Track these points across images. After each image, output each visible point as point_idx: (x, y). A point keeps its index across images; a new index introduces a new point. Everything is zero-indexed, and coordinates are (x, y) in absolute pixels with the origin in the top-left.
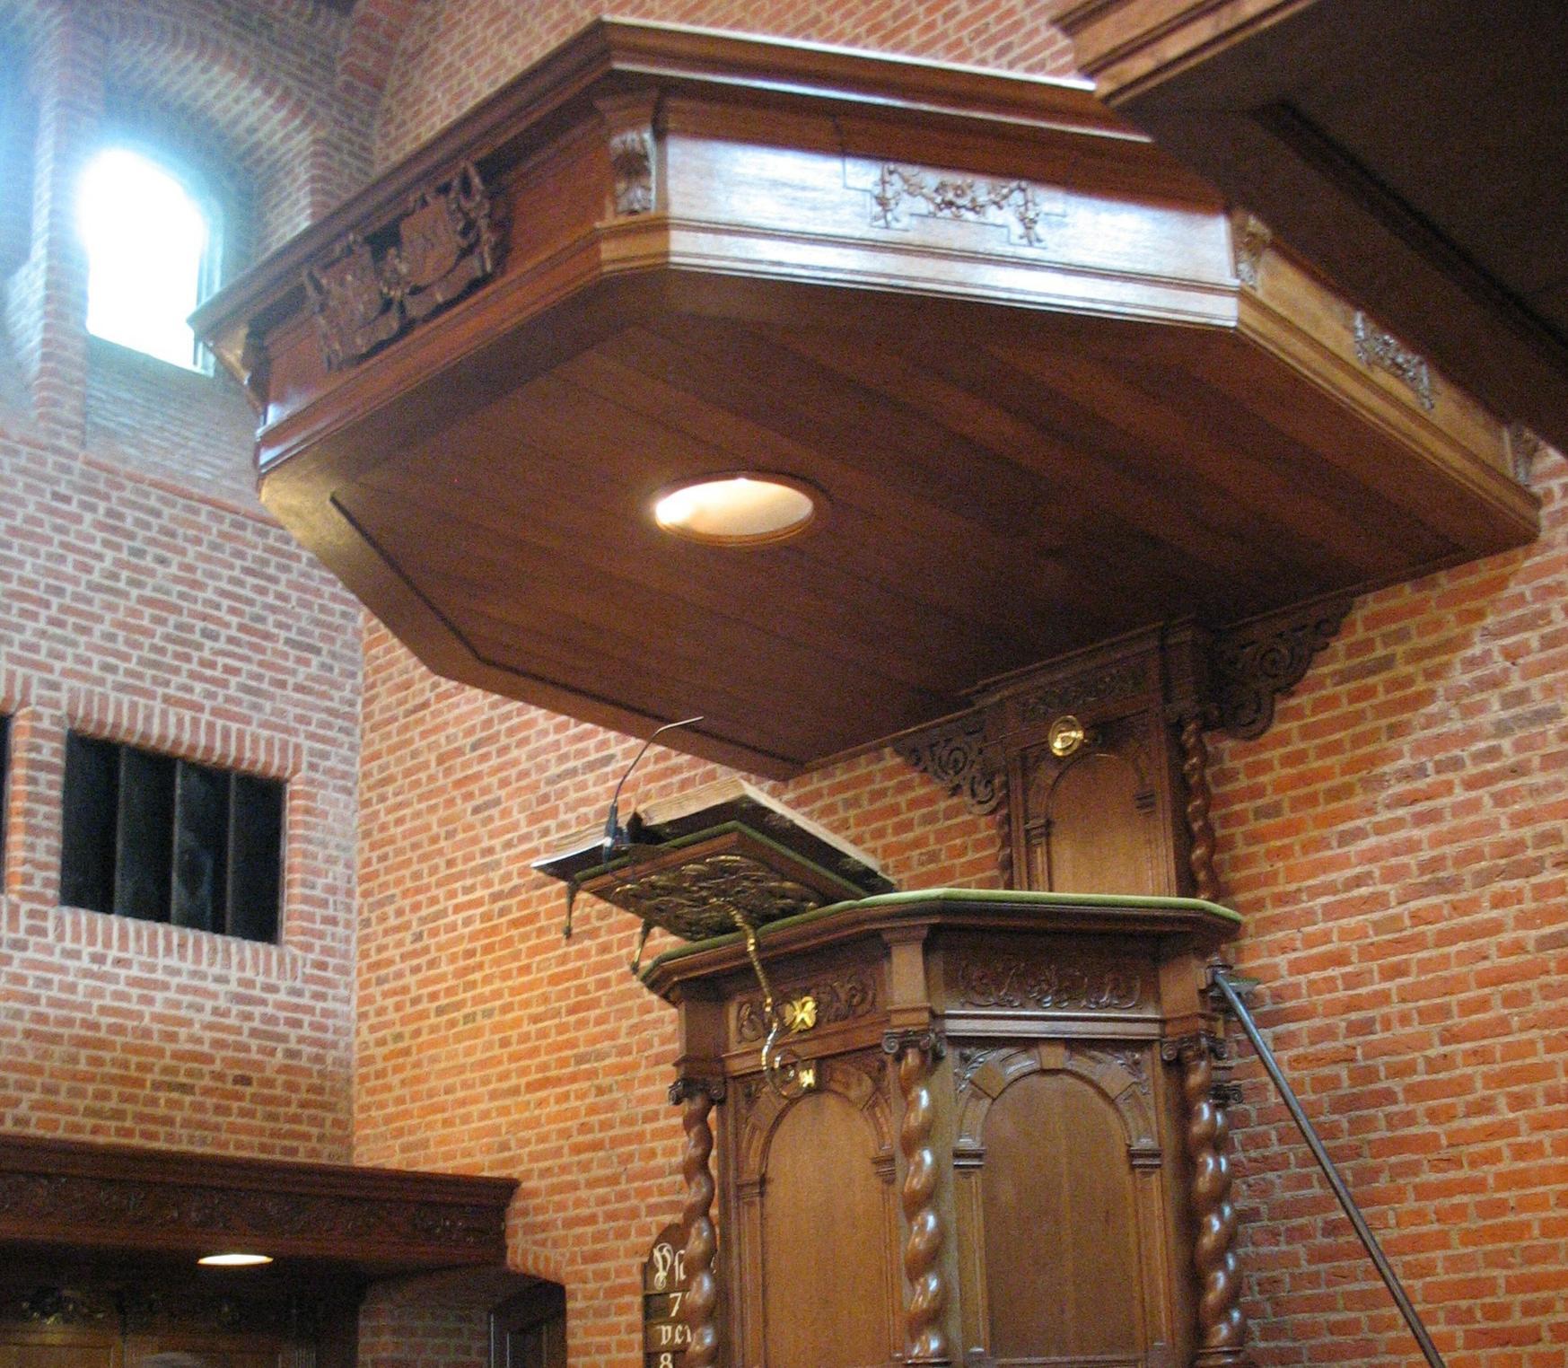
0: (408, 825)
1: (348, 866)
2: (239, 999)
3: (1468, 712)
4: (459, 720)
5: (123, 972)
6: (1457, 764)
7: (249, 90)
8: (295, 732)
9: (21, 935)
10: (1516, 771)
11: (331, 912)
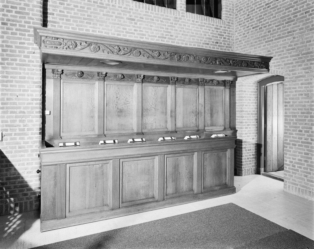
1: (233, 5)
2: (216, 28)
5: (197, 24)
9: (180, 17)
11: (230, 13)
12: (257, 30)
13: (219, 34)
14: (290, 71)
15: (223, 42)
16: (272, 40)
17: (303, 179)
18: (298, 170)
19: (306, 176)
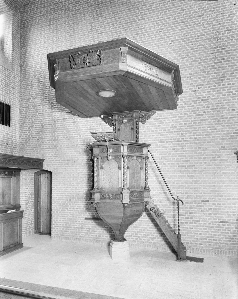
0: (27, 114)
2: (6, 134)
3: (167, 125)
4: (36, 102)
6: (166, 130)
7: (3, 3)
8: (12, 99)
10: (172, 132)
12: (35, 140)
13: (8, 138)
14: (55, 169)
15: (11, 144)
16: (45, 149)
17: (61, 231)
18: (59, 227)
19: (63, 229)
